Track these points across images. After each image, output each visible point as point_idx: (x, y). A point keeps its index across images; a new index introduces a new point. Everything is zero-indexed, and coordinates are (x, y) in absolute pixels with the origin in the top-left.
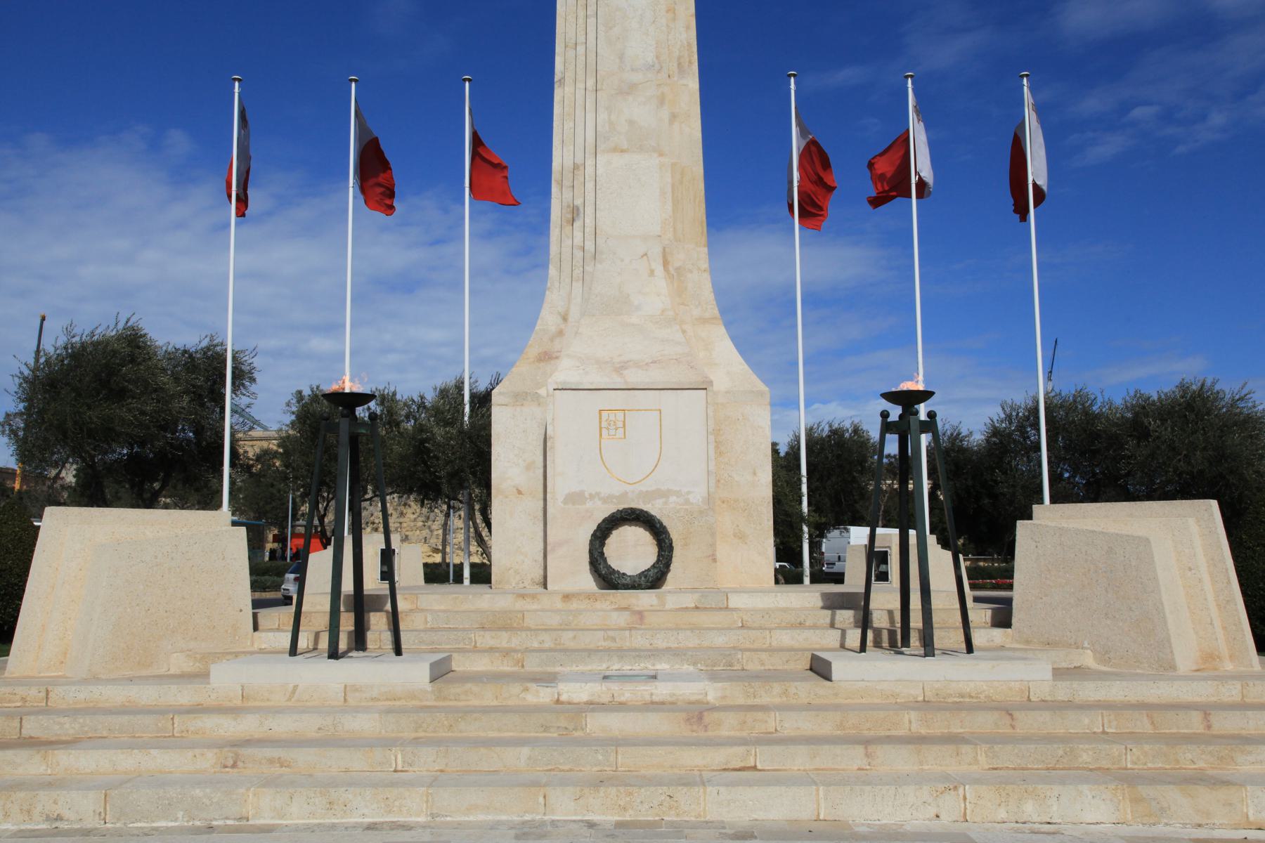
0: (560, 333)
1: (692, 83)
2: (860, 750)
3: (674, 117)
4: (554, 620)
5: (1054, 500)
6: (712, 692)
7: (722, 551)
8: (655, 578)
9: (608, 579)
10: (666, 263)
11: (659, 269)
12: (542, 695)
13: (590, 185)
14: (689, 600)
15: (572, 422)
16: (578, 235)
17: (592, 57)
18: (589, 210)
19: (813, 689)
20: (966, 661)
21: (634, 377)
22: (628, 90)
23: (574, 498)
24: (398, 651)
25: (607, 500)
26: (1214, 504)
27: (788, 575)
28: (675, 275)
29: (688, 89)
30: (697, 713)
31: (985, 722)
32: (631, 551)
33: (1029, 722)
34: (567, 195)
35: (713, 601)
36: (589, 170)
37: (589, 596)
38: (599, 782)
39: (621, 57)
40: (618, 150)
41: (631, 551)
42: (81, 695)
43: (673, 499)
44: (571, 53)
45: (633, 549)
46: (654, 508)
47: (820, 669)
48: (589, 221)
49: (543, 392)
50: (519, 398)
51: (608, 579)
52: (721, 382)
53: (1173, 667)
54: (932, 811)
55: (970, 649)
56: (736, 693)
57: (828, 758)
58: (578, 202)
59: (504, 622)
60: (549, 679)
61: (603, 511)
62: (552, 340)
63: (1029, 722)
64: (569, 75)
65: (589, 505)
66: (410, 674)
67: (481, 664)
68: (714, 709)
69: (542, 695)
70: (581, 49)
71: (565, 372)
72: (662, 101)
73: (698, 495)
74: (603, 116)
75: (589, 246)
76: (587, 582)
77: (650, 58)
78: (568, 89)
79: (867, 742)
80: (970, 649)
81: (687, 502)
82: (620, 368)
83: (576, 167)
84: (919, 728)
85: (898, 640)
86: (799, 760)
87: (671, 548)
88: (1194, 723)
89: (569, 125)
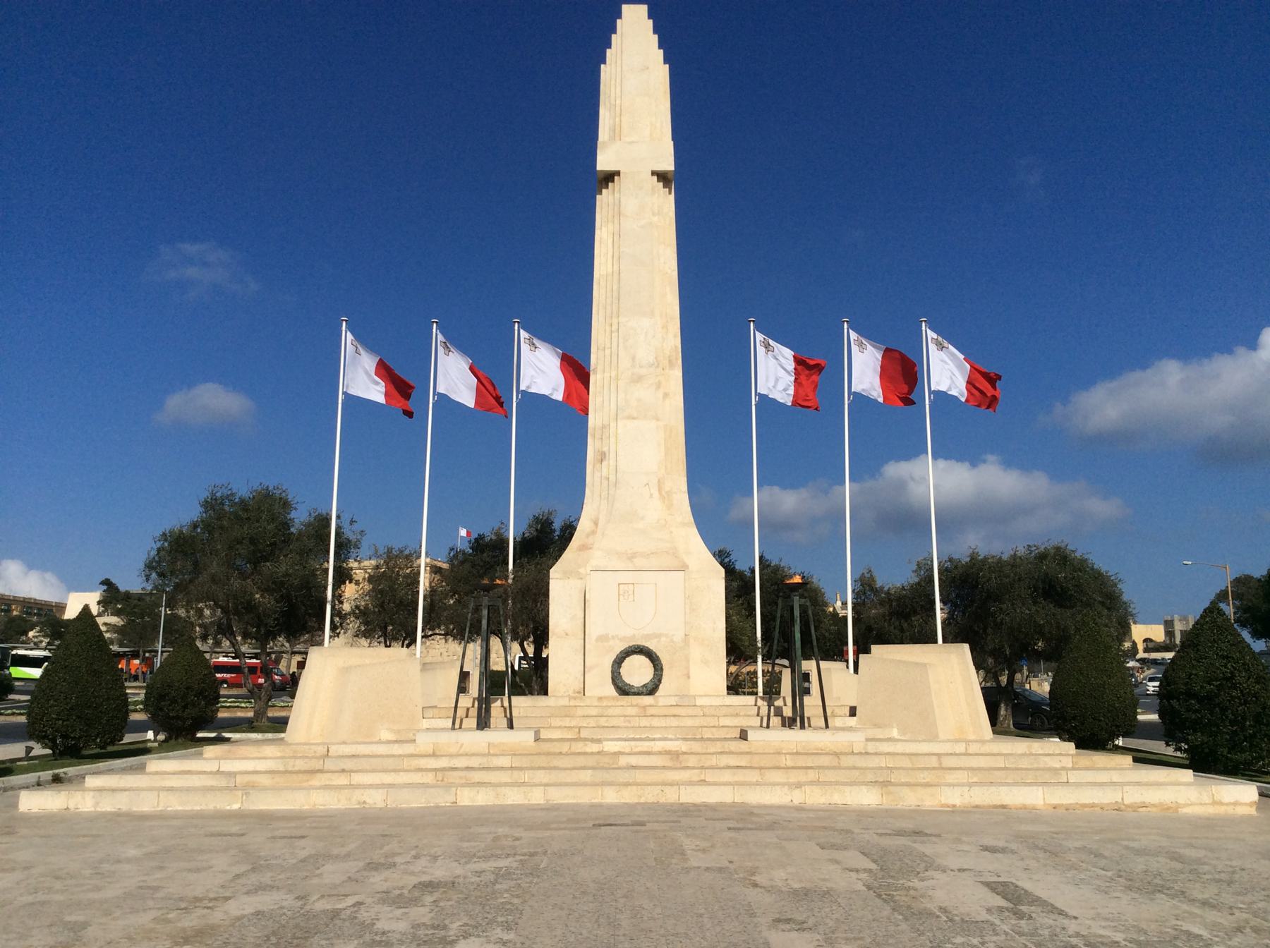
0: (594, 532)
1: (678, 373)
2: (757, 771)
3: (666, 395)
4: (594, 712)
5: (945, 641)
6: (683, 746)
7: (694, 671)
8: (651, 689)
9: (624, 690)
10: (660, 490)
11: (656, 494)
12: (594, 748)
13: (612, 440)
14: (673, 701)
15: (601, 589)
16: (605, 471)
17: (614, 358)
18: (612, 455)
19: (743, 746)
20: (828, 732)
21: (639, 562)
22: (638, 379)
23: (602, 638)
24: (511, 726)
25: (622, 639)
26: (966, 647)
27: (735, 687)
28: (666, 497)
29: (675, 379)
30: (675, 755)
31: (825, 761)
32: (636, 670)
33: (847, 761)
34: (598, 443)
35: (685, 700)
36: (612, 429)
37: (613, 698)
38: (627, 784)
39: (634, 359)
40: (631, 418)
41: (636, 670)
42: (347, 750)
43: (663, 639)
44: (601, 353)
45: (639, 671)
46: (651, 645)
47: (743, 736)
48: (612, 462)
49: (582, 571)
50: (567, 575)
51: (624, 690)
52: (692, 563)
53: (937, 736)
54: (789, 799)
55: (827, 727)
56: (696, 747)
57: (740, 776)
58: (605, 449)
59: (566, 712)
60: (599, 741)
61: (620, 647)
62: (588, 536)
63: (847, 761)
64: (600, 368)
65: (611, 643)
66: (522, 737)
67: (556, 735)
68: (685, 753)
69: (594, 748)
70: (607, 352)
71: (598, 558)
72: (659, 386)
73: (678, 637)
74: (621, 396)
75: (612, 478)
76: (612, 691)
77: (651, 359)
78: (599, 376)
79: (761, 768)
80: (827, 727)
81: (672, 641)
82: (632, 557)
83: (603, 427)
84: (789, 763)
85: (789, 723)
86: (727, 776)
87: (662, 669)
88: (934, 762)
89: (599, 400)
